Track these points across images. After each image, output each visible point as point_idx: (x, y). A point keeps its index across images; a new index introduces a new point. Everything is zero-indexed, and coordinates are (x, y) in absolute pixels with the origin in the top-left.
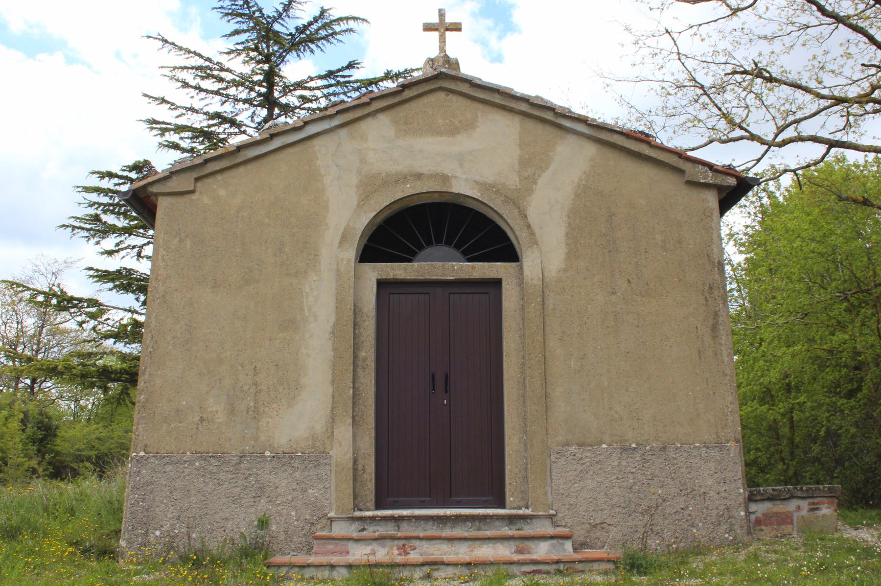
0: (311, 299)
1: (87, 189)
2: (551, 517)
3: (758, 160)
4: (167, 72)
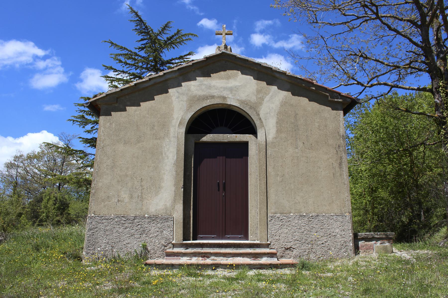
0: (166, 149)
1: (79, 105)
3: (361, 93)
4: (113, 56)
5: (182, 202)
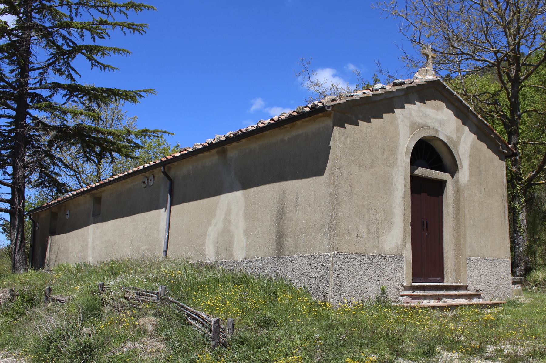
0: (395, 180)
5: (411, 241)
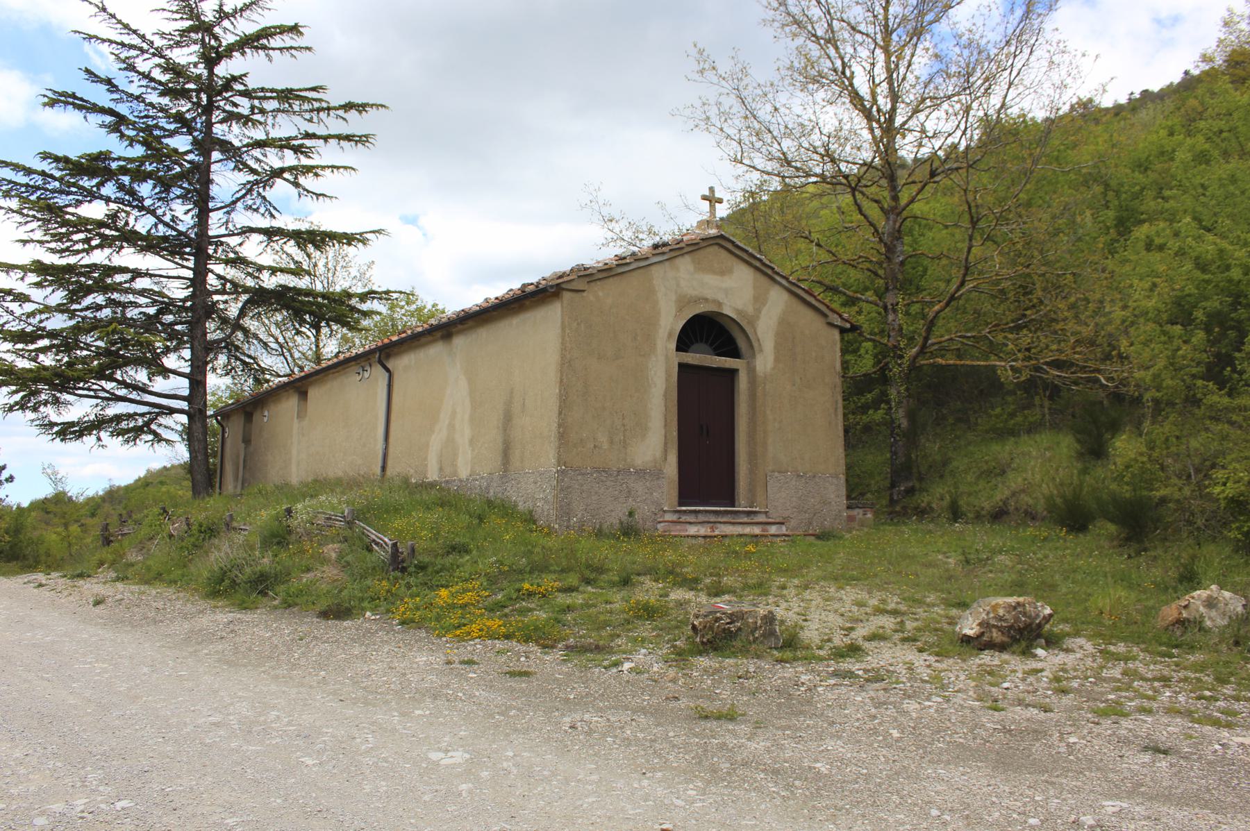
2: (766, 513)
